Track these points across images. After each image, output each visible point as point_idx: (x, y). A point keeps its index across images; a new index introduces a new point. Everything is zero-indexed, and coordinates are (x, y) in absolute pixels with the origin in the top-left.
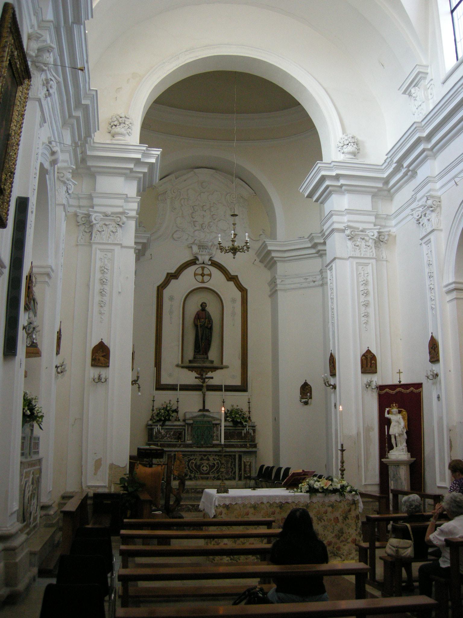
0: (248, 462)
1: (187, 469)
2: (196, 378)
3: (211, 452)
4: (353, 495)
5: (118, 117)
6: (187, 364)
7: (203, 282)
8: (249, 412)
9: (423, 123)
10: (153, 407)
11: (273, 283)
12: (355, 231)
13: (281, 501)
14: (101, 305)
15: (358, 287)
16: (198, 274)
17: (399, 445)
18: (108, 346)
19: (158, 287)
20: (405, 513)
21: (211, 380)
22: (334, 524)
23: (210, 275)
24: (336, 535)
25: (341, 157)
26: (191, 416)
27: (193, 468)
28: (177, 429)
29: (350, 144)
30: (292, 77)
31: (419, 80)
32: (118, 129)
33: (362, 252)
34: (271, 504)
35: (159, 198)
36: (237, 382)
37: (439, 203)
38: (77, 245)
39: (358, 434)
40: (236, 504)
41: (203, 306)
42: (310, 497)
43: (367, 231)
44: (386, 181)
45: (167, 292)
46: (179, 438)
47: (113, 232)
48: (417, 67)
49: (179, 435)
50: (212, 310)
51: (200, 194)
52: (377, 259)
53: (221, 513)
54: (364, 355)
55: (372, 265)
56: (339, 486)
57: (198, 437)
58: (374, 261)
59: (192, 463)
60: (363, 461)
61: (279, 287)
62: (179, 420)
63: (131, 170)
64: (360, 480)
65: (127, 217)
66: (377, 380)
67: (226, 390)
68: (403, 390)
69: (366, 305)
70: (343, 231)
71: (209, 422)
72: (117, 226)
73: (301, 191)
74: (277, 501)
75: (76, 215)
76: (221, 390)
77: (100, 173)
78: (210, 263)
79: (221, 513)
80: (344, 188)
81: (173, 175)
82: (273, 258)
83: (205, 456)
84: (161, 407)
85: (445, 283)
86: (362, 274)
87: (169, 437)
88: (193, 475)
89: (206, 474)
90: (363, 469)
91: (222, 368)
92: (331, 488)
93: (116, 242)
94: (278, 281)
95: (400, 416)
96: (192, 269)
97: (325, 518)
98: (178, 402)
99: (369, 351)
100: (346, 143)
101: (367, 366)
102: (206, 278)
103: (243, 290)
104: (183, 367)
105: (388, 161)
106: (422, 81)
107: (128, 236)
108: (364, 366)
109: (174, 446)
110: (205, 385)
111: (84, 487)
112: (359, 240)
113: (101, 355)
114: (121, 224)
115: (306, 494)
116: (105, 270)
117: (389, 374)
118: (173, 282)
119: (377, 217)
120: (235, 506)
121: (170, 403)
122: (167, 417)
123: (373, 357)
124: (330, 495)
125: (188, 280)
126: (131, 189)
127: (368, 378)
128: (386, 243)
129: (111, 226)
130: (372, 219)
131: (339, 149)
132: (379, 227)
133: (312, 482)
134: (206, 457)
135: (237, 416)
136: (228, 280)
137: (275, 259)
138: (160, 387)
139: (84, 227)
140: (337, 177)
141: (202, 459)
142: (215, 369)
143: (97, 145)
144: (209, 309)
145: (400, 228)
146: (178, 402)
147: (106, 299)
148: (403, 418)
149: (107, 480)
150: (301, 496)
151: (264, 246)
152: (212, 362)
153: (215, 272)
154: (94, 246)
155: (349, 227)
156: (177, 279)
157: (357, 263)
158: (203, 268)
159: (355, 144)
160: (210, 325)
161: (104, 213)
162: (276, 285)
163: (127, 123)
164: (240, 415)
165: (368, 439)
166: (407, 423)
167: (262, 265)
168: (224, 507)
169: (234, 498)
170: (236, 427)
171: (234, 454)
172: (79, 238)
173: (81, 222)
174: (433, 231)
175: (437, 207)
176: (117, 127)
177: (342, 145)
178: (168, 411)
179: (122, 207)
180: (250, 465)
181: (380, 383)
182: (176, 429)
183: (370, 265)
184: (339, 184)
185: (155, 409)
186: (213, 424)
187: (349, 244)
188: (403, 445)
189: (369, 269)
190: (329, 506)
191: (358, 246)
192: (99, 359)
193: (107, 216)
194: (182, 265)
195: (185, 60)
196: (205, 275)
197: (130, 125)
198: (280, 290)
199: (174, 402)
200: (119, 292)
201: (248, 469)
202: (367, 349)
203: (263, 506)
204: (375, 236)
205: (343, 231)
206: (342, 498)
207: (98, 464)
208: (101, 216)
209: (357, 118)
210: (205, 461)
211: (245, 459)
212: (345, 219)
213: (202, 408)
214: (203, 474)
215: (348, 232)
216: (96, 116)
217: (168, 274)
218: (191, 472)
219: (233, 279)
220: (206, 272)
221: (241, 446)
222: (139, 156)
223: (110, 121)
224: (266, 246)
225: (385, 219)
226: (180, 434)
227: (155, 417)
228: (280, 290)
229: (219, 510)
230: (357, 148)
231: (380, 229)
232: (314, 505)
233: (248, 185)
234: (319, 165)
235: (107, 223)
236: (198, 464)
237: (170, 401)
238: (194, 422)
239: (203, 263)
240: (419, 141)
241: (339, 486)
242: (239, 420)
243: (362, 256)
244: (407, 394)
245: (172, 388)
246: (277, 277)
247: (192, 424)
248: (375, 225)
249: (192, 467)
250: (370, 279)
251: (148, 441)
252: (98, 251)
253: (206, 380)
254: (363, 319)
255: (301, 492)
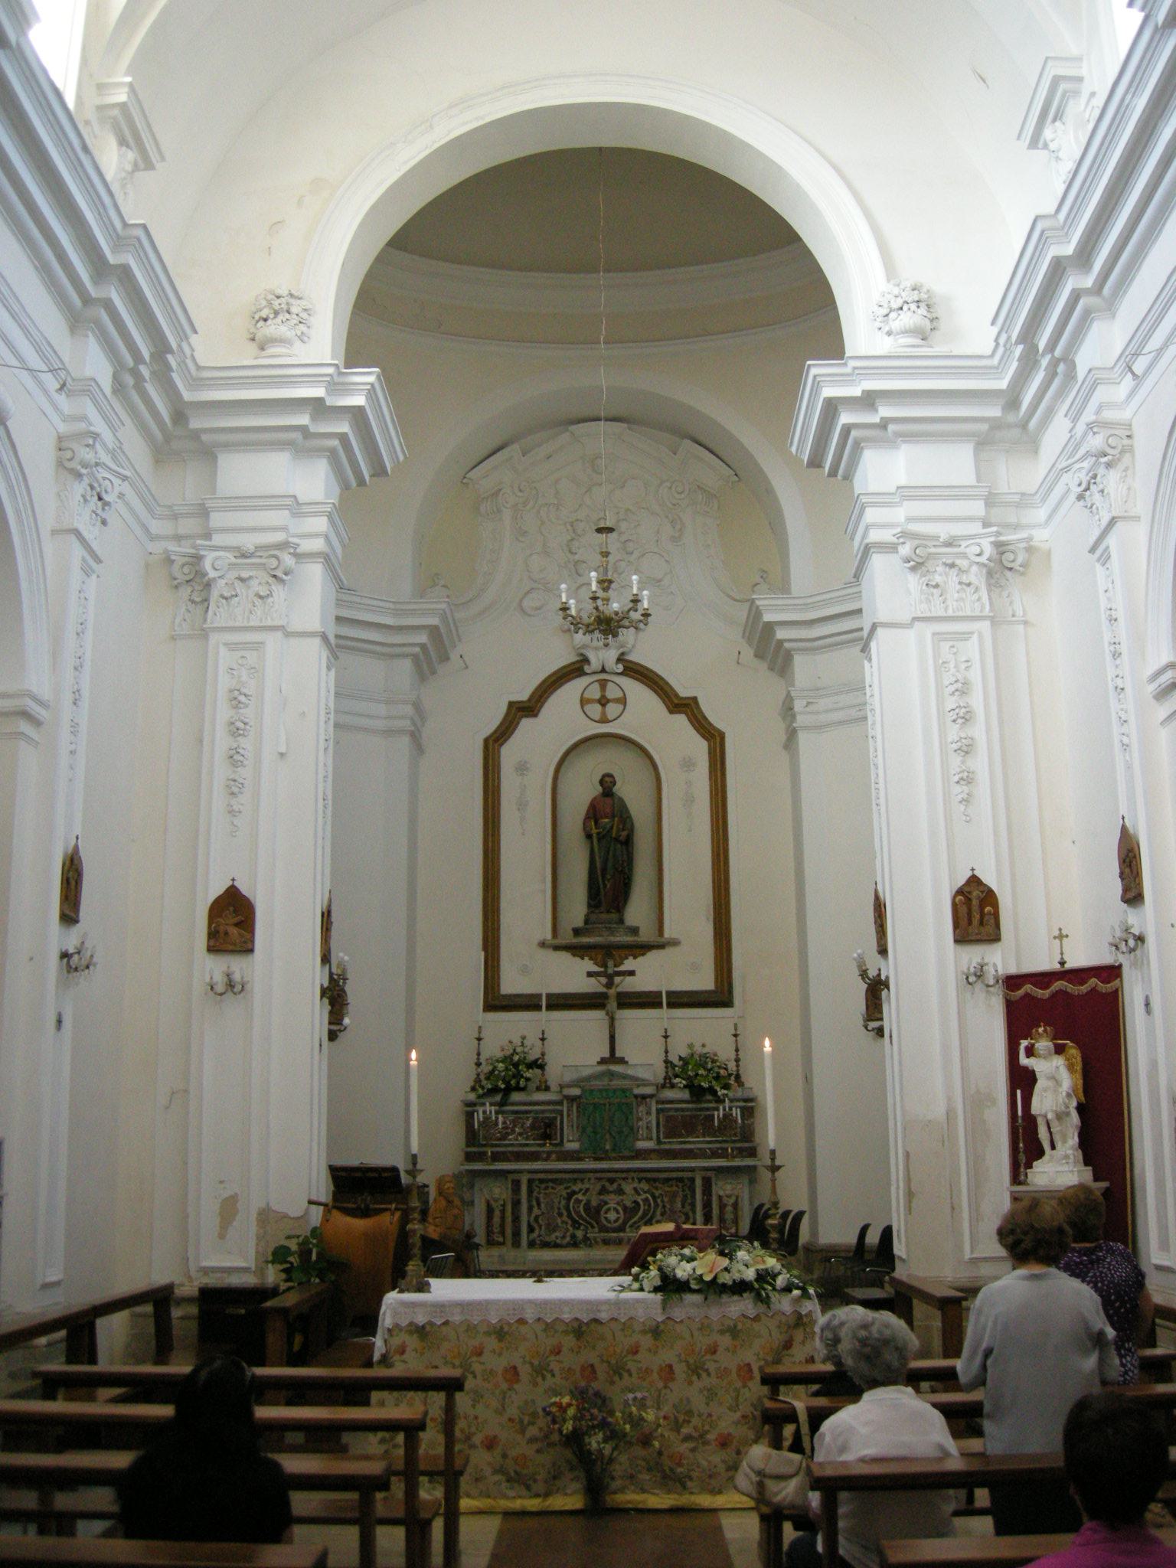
0: (729, 1196)
1: (565, 1218)
2: (590, 974)
3: (628, 1170)
4: (798, 1300)
5: (271, 297)
6: (568, 938)
7: (604, 720)
8: (737, 1060)
9: (1062, 216)
10: (479, 1054)
11: (788, 710)
12: (925, 546)
13: (579, 1316)
14: (234, 788)
15: (940, 701)
16: (590, 701)
17: (1059, 1145)
18: (251, 898)
19: (486, 741)
20: (824, 1362)
21: (629, 979)
22: (739, 1384)
23: (623, 700)
24: (744, 1417)
25: (884, 345)
26: (575, 1076)
27: (580, 1216)
28: (543, 1112)
29: (905, 308)
30: (742, 142)
31: (1061, 101)
32: (272, 329)
33: (949, 602)
34: (547, 1324)
35: (483, 509)
36: (704, 981)
37: (1126, 442)
38: (173, 638)
39: (950, 1114)
40: (446, 1323)
41: (607, 784)
42: (665, 1305)
43: (964, 544)
44: (1011, 399)
45: (509, 753)
46: (546, 1136)
47: (261, 597)
48: (1050, 63)
49: (547, 1129)
50: (632, 792)
51: (589, 490)
52: (995, 621)
53: (402, 1351)
54: (960, 892)
55: (980, 633)
56: (750, 1274)
57: (595, 1133)
58: (985, 626)
59: (578, 1201)
60: (964, 1190)
61: (801, 720)
62: (547, 1089)
63: (303, 429)
64: (959, 1247)
65: (295, 555)
66: (1001, 960)
67: (671, 1005)
68: (1071, 988)
69: (966, 750)
70: (892, 548)
71: (624, 1091)
72: (271, 580)
73: (794, 449)
74: (567, 1317)
75: (169, 561)
76: (538, 1008)
77: (227, 446)
78: (620, 668)
79: (402, 1351)
80: (891, 427)
81: (515, 447)
82: (781, 642)
83: (610, 1181)
84: (499, 1055)
85: (1150, 671)
86: (952, 665)
87: (520, 1134)
88: (580, 1234)
89: (615, 1230)
90: (966, 1215)
91: (662, 946)
92: (726, 1279)
93: (269, 623)
94: (798, 705)
95: (1059, 1062)
96: (572, 690)
97: (711, 1366)
98: (543, 1039)
99: (974, 881)
100: (895, 306)
101: (970, 923)
102: (612, 710)
103: (713, 736)
104: (556, 948)
105: (1002, 341)
106: (1071, 102)
107: (309, 600)
108: (964, 922)
109: (534, 1157)
110: (612, 992)
111: (193, 1273)
112: (940, 569)
113: (232, 921)
114: (279, 574)
115: (652, 1295)
116: (242, 698)
117: (1031, 944)
118: (526, 726)
119: (990, 501)
120: (444, 1329)
121: (523, 1045)
122: (513, 1082)
123: (989, 897)
124: (725, 1298)
125: (565, 717)
126: (313, 482)
127: (974, 955)
128: (1022, 574)
129: (254, 583)
130: (978, 508)
131: (878, 324)
132: (995, 529)
133: (673, 1260)
134: (615, 1186)
135: (701, 1072)
136: (671, 712)
137: (787, 645)
138: (496, 1002)
139: (189, 589)
140: (869, 400)
141: (603, 1191)
142: (643, 949)
143: (206, 374)
144: (620, 789)
145: (1053, 529)
146: (543, 1039)
147: (245, 773)
148: (1070, 1068)
149: (252, 1252)
150: (638, 1301)
151: (755, 613)
152: (635, 931)
153: (635, 690)
154: (214, 638)
155: (906, 535)
156: (536, 716)
157: (934, 634)
158: (603, 684)
159: (923, 305)
160: (625, 833)
161: (238, 548)
162: (794, 716)
163: (294, 310)
164: (709, 1070)
165: (977, 1129)
166: (1080, 1082)
167: (763, 666)
168: (411, 1333)
169: (440, 1307)
170: (698, 1101)
171: (690, 1175)
172: (177, 621)
173: (181, 578)
174: (1113, 522)
175: (1122, 452)
176: (269, 322)
177: (885, 311)
178: (516, 1065)
179: (284, 529)
180: (735, 1205)
181: (1013, 970)
182: (537, 1112)
183: (975, 637)
184: (877, 420)
185: (482, 1060)
186: (636, 1097)
187: (913, 581)
188: (1069, 1143)
189: (971, 649)
190: (722, 1332)
191: (937, 586)
192: (226, 933)
193: (244, 556)
194: (550, 676)
195: (450, 132)
196: (608, 701)
197: (304, 315)
198: (806, 728)
199: (533, 1039)
200: (282, 755)
201: (729, 1216)
202: (970, 874)
203: (523, 1329)
204: (987, 555)
205: (892, 548)
206: (762, 1308)
207: (229, 1209)
208: (230, 557)
209: (916, 228)
210: (613, 1196)
211: (723, 1188)
212: (899, 514)
213: (607, 1055)
214: (607, 1230)
215: (905, 550)
216: (171, 295)
217: (511, 704)
218: (576, 1225)
219: (684, 706)
220: (612, 692)
221: (715, 1154)
222: (319, 392)
223: (254, 309)
224: (758, 614)
225: (1018, 505)
226: (550, 1124)
227: (484, 1082)
228: (806, 728)
229: (396, 1341)
230: (929, 314)
231: (999, 534)
232: (679, 1328)
233: (711, 452)
234: (814, 371)
235: (244, 574)
236: (594, 1203)
237: (524, 1038)
238: (584, 1091)
239: (603, 670)
240: (1058, 269)
241: (750, 1274)
242: (705, 1085)
243: (950, 613)
244: (1081, 997)
245: (528, 1003)
246: (793, 694)
247: (579, 1097)
248: (986, 524)
249: (578, 1213)
250: (975, 676)
251: (468, 1146)
252: (223, 650)
253: (617, 979)
254: (957, 789)
255: (641, 1289)
